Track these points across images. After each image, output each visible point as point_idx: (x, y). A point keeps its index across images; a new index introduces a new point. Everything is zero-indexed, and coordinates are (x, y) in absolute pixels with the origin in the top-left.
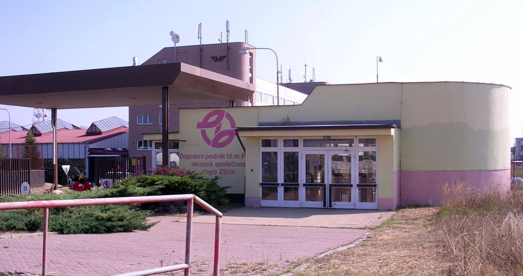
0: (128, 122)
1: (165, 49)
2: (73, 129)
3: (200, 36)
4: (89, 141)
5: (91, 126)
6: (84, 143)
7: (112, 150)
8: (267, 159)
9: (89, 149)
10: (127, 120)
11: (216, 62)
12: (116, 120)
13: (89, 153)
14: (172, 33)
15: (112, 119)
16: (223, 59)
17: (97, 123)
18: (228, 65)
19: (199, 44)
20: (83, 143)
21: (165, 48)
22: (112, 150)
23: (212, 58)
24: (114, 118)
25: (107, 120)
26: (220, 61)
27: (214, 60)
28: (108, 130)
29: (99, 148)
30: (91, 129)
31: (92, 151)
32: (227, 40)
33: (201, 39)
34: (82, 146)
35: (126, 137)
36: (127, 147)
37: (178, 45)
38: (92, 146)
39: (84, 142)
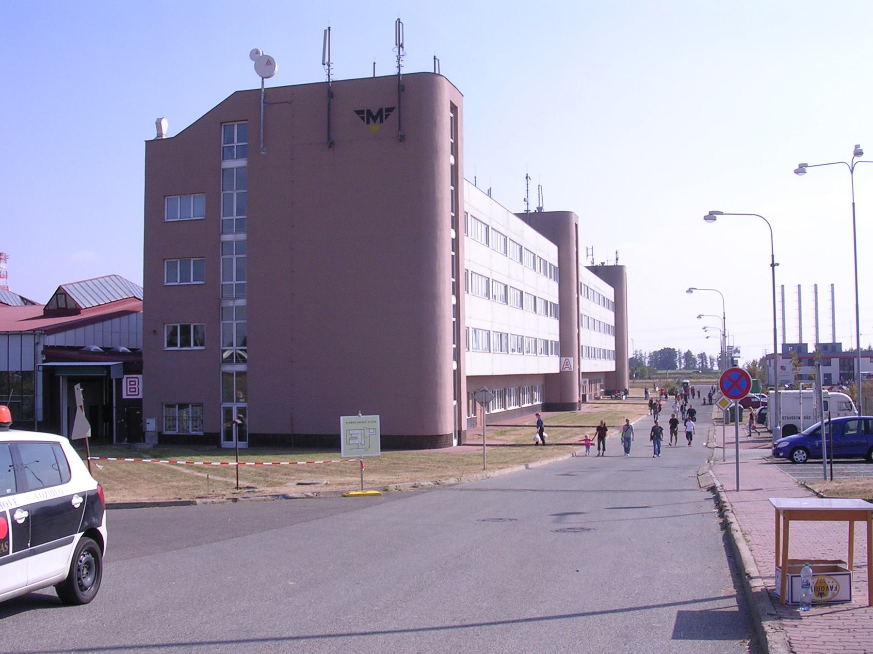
0: (142, 287)
1: (238, 96)
2: (22, 306)
3: (327, 60)
4: (46, 329)
5: (56, 294)
6: (33, 332)
7: (129, 351)
8: (789, 384)
9: (45, 347)
10: (141, 284)
11: (368, 123)
12: (117, 281)
13: (44, 358)
14: (255, 54)
15: (108, 279)
16: (387, 116)
17: (70, 287)
18: (399, 129)
19: (323, 79)
20: (31, 334)
21: (236, 92)
22: (129, 351)
23: (359, 112)
24: (113, 278)
25: (96, 282)
26: (379, 119)
27: (363, 118)
28: (95, 304)
29: (72, 345)
30: (55, 300)
31: (51, 353)
32: (399, 67)
33: (329, 66)
34: (29, 341)
35: (136, 323)
36: (140, 346)
37: (270, 83)
38: (51, 340)
39: (34, 330)
